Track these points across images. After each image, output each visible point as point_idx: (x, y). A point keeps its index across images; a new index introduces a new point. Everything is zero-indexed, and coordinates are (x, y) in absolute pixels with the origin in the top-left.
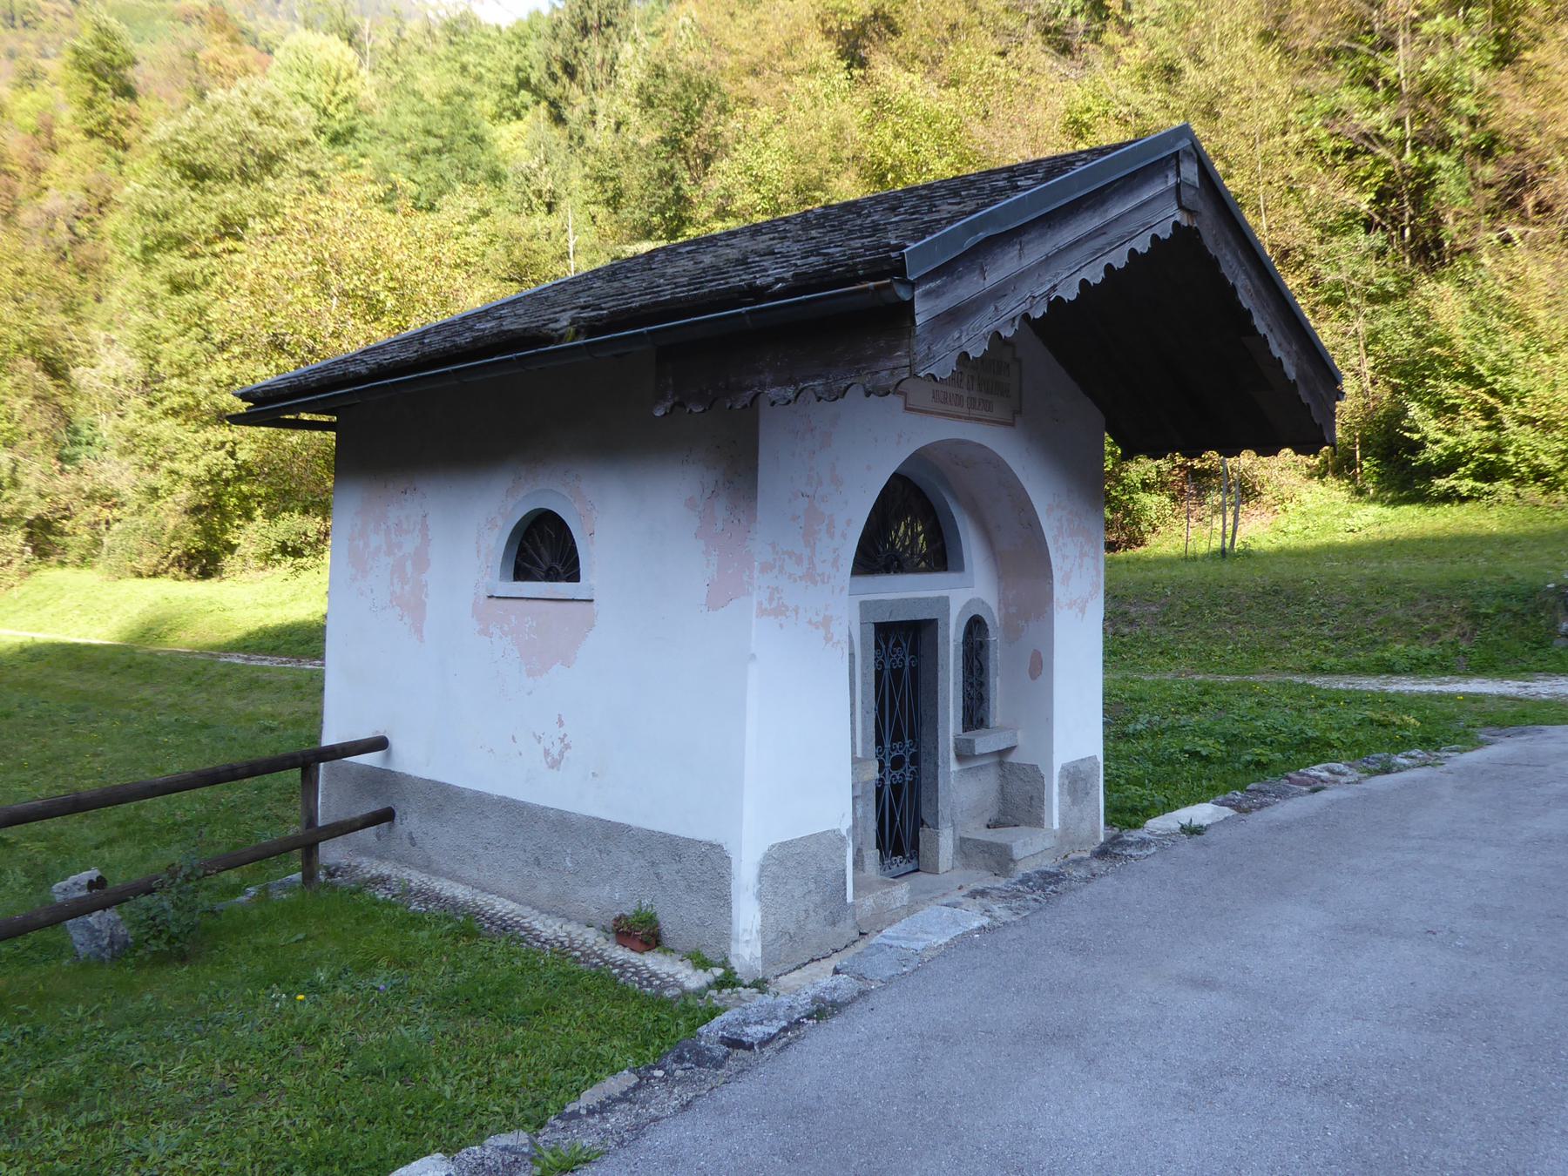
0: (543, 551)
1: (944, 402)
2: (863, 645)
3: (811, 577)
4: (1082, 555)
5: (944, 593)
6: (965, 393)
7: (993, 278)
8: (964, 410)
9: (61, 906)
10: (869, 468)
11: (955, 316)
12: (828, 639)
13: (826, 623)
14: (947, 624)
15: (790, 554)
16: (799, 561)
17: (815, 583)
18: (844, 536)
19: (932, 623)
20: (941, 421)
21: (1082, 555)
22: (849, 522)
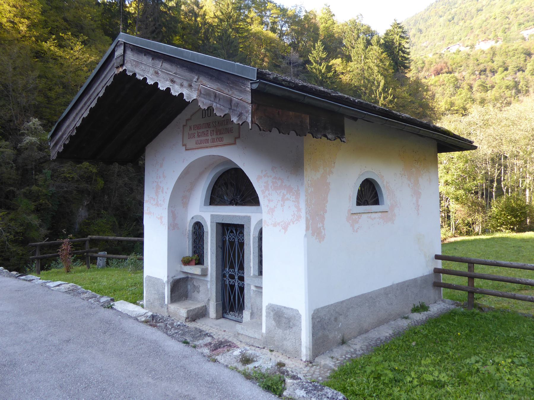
0: (369, 194)
1: (201, 143)
2: (212, 229)
3: (157, 205)
4: (283, 200)
5: (248, 215)
6: (209, 138)
7: (63, 131)
8: (210, 144)
9: (441, 283)
10: (174, 171)
11: (56, 144)
12: (161, 223)
13: (161, 218)
14: (249, 228)
15: (152, 198)
16: (154, 200)
17: (158, 206)
18: (166, 193)
19: (242, 227)
20: (200, 150)
21: (283, 200)
22: (168, 189)
